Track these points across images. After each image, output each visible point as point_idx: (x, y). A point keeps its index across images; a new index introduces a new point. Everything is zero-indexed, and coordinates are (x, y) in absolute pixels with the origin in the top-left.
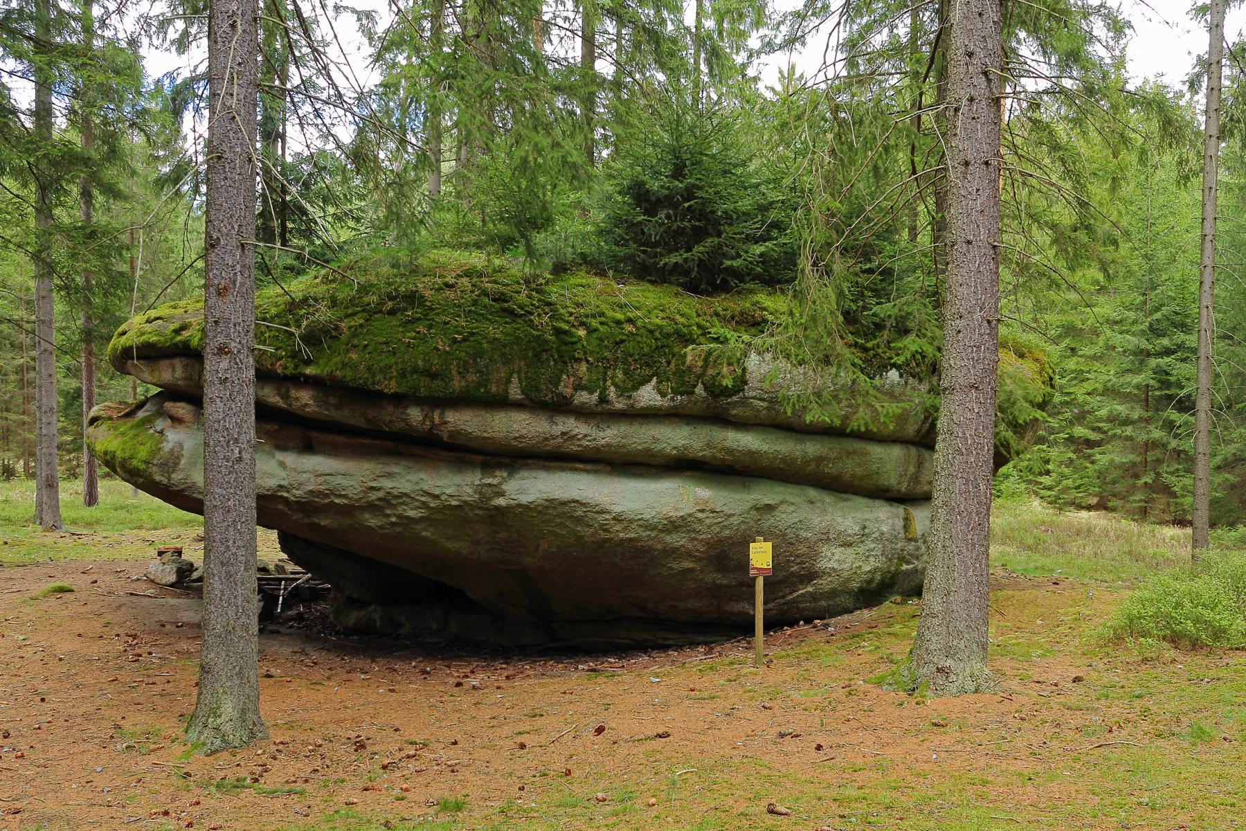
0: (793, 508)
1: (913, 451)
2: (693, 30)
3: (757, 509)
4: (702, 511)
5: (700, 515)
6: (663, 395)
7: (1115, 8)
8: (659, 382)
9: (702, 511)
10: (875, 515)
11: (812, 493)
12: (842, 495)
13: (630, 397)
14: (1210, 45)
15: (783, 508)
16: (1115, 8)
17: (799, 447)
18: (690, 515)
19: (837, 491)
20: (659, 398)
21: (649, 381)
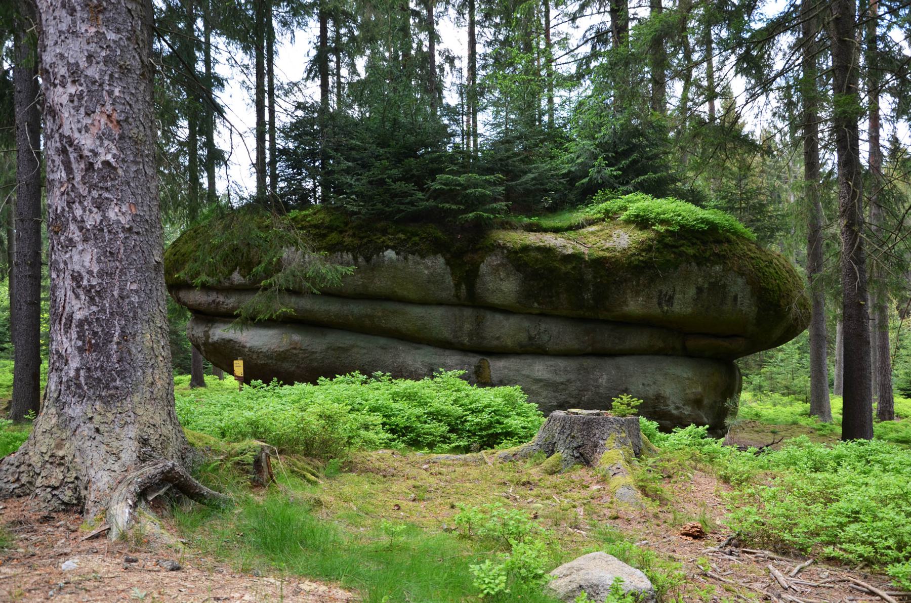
0: (365, 351)
1: (456, 311)
2: (705, 83)
3: (334, 350)
4: (295, 348)
5: (294, 351)
6: (244, 277)
7: (735, 96)
8: (240, 269)
9: (295, 348)
10: (443, 361)
11: (382, 341)
12: (414, 345)
13: (229, 279)
14: (257, 187)
15: (355, 350)
16: (735, 96)
17: (345, 308)
18: (287, 351)
19: (367, 334)
20: (242, 279)
21: (236, 269)
